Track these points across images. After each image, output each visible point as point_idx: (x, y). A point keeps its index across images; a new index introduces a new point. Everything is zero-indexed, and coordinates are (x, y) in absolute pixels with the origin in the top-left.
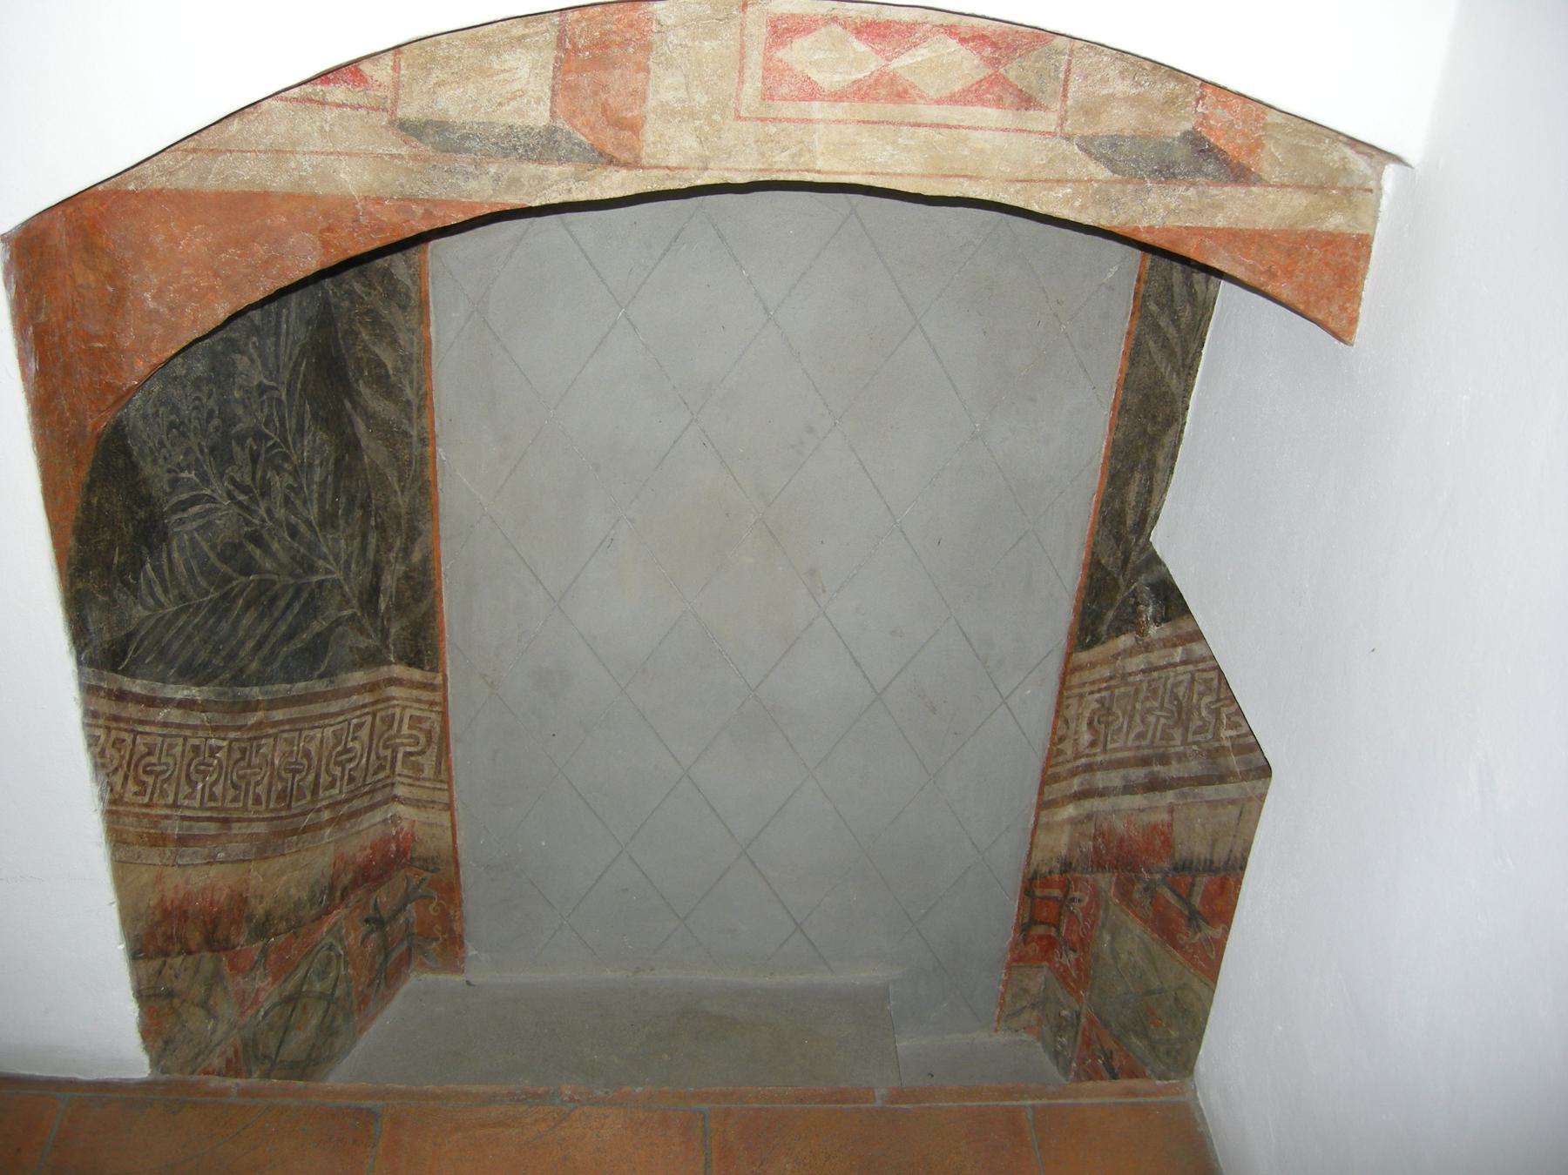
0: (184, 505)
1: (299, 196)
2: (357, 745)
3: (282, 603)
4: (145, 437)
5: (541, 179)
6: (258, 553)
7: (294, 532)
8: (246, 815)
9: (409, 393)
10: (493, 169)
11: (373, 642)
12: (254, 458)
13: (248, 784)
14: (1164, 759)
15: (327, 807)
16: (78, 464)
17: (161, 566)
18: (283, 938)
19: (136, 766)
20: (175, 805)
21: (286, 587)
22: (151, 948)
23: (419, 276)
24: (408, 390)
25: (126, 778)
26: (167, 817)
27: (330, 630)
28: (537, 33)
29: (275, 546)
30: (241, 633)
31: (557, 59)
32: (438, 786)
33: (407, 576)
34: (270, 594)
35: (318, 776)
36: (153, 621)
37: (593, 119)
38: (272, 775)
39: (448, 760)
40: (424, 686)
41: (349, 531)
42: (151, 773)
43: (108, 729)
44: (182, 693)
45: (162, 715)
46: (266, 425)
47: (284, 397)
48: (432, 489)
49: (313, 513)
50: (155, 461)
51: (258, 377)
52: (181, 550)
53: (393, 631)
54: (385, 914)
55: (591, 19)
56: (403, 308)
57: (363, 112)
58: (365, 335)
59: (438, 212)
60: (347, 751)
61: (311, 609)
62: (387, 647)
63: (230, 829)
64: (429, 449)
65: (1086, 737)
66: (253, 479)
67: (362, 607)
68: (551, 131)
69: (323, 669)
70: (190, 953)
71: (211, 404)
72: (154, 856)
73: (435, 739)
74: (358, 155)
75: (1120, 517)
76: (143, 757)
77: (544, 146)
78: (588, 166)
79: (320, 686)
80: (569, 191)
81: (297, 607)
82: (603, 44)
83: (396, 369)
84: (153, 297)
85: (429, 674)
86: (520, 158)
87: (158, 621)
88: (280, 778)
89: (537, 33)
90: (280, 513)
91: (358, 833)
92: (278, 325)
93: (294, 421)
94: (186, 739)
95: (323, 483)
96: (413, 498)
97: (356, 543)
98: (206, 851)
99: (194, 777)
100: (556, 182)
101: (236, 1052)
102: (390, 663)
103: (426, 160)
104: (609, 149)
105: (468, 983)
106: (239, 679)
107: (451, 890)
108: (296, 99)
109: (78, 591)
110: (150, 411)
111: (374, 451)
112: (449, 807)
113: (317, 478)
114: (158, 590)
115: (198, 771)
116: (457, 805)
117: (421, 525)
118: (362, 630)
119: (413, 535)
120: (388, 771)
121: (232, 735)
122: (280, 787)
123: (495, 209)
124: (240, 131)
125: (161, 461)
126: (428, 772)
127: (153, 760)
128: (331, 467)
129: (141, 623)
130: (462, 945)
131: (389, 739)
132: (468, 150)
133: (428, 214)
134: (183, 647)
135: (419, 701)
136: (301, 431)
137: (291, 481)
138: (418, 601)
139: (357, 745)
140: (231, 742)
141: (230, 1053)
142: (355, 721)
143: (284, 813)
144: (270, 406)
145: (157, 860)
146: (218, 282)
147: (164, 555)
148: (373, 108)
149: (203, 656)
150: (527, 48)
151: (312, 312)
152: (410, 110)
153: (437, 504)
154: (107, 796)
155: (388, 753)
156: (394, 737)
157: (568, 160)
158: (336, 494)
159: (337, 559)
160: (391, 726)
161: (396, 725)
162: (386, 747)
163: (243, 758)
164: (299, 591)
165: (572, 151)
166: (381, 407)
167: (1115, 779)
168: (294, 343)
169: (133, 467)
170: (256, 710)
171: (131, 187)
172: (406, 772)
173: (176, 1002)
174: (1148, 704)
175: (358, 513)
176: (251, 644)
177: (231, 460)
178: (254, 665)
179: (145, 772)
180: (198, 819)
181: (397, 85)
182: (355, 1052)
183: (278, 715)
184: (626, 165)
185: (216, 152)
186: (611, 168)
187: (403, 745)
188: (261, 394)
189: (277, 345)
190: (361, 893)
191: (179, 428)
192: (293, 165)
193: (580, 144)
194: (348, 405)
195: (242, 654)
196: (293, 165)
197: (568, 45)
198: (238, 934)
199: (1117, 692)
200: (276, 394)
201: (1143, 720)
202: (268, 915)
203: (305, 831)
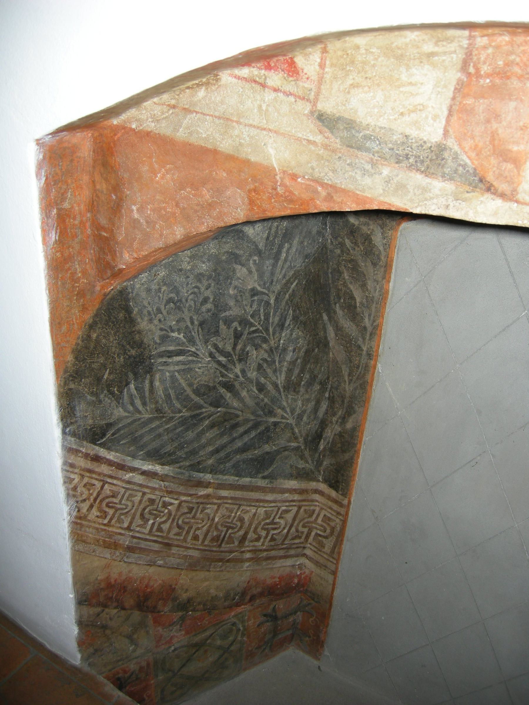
0: (170, 354)
1: (237, 158)
2: (282, 522)
3: (241, 430)
4: (145, 303)
5: (425, 190)
6: (228, 395)
7: (261, 388)
8: (184, 544)
9: (367, 322)
10: (386, 171)
11: (310, 466)
12: (237, 336)
13: (190, 528)
15: (250, 551)
16: (84, 309)
17: (143, 388)
18: (198, 614)
19: (101, 501)
20: (128, 528)
21: (247, 421)
22: (94, 601)
23: (388, 246)
24: (366, 320)
25: (91, 506)
26: (120, 534)
27: (278, 452)
28: (445, 53)
29: (244, 393)
30: (203, 441)
31: (459, 81)
32: (331, 559)
33: (340, 435)
34: (233, 422)
35: (246, 533)
36: (129, 420)
37: (481, 144)
38: (210, 526)
39: (340, 548)
40: (336, 502)
41: (307, 396)
42: (112, 507)
43: (82, 476)
44: (147, 467)
45: (128, 476)
46: (252, 316)
47: (272, 301)
48: (368, 388)
49: (281, 379)
50: (151, 321)
51: (252, 283)
52: (162, 381)
53: (325, 463)
54: (279, 614)
55: (498, 47)
56: (374, 264)
57: (292, 99)
58: (346, 275)
59: (337, 197)
60: (273, 523)
61: (266, 436)
62: (319, 471)
63: (170, 549)
64: (372, 362)
66: (234, 348)
67: (306, 442)
68: (441, 148)
69: (266, 473)
70: (123, 609)
71: (208, 293)
72: (107, 554)
73: (336, 533)
74: (283, 134)
76: (107, 497)
77: (431, 160)
78: (467, 188)
79: (261, 483)
80: (447, 207)
81: (253, 434)
82: (504, 74)
83: (361, 303)
84: (138, 210)
85: (340, 497)
86: (410, 167)
87: (135, 421)
88: (217, 529)
89: (445, 53)
90: (253, 374)
91: (272, 568)
92: (279, 253)
93: (277, 319)
94: (144, 494)
95: (293, 363)
96: (355, 389)
97: (311, 406)
98: (149, 558)
99: (147, 516)
100: (437, 196)
101: (148, 665)
102: (318, 481)
103: (334, 151)
104: (490, 177)
105: (319, 667)
106: (196, 467)
107: (324, 616)
108: (245, 79)
109: (70, 389)
110: (154, 287)
111: (336, 351)
112: (334, 573)
113: (288, 358)
114: (138, 402)
115: (150, 513)
116: (339, 574)
117: (356, 408)
118: (302, 457)
119: (350, 412)
120: (302, 540)
121: (184, 498)
122: (215, 533)
123: (382, 208)
124: (204, 98)
125: (156, 322)
126: (327, 549)
127: (115, 500)
128: (302, 354)
129: (120, 419)
130: (322, 646)
131: (308, 522)
132: (368, 150)
133: (329, 198)
134: (153, 440)
135: (331, 508)
136: (281, 326)
137: (266, 356)
138: (344, 452)
139: (282, 522)
140: (181, 502)
141: (144, 664)
142: (284, 508)
143: (214, 549)
144: (259, 305)
145: (108, 556)
146: (178, 211)
147: (147, 382)
148: (299, 97)
149: (169, 448)
150: (434, 66)
151: (311, 249)
152: (327, 106)
153: (369, 398)
154: (75, 514)
155: (306, 530)
156: (312, 522)
157: (451, 179)
158: (302, 371)
159: (293, 411)
160: (311, 516)
161: (315, 516)
162: (304, 526)
163: (190, 512)
164: (256, 426)
165: (456, 171)
166: (347, 325)
168: (290, 267)
169: (131, 321)
170: (207, 487)
171: (134, 126)
172: (314, 544)
173: (108, 632)
175: (317, 387)
176: (211, 449)
177: (217, 333)
178: (210, 462)
179: (107, 505)
180: (146, 540)
181: (321, 80)
182: (237, 680)
183: (224, 493)
184: (503, 196)
185: (187, 111)
186: (488, 196)
187: (316, 528)
188: (253, 296)
189: (274, 266)
190: (264, 600)
191: (177, 304)
192: (236, 132)
193: (464, 166)
194: (325, 317)
195: (202, 453)
196: (236, 132)
197: (472, 70)
198: (164, 605)
200: (265, 298)
202: (189, 600)
203: (228, 561)
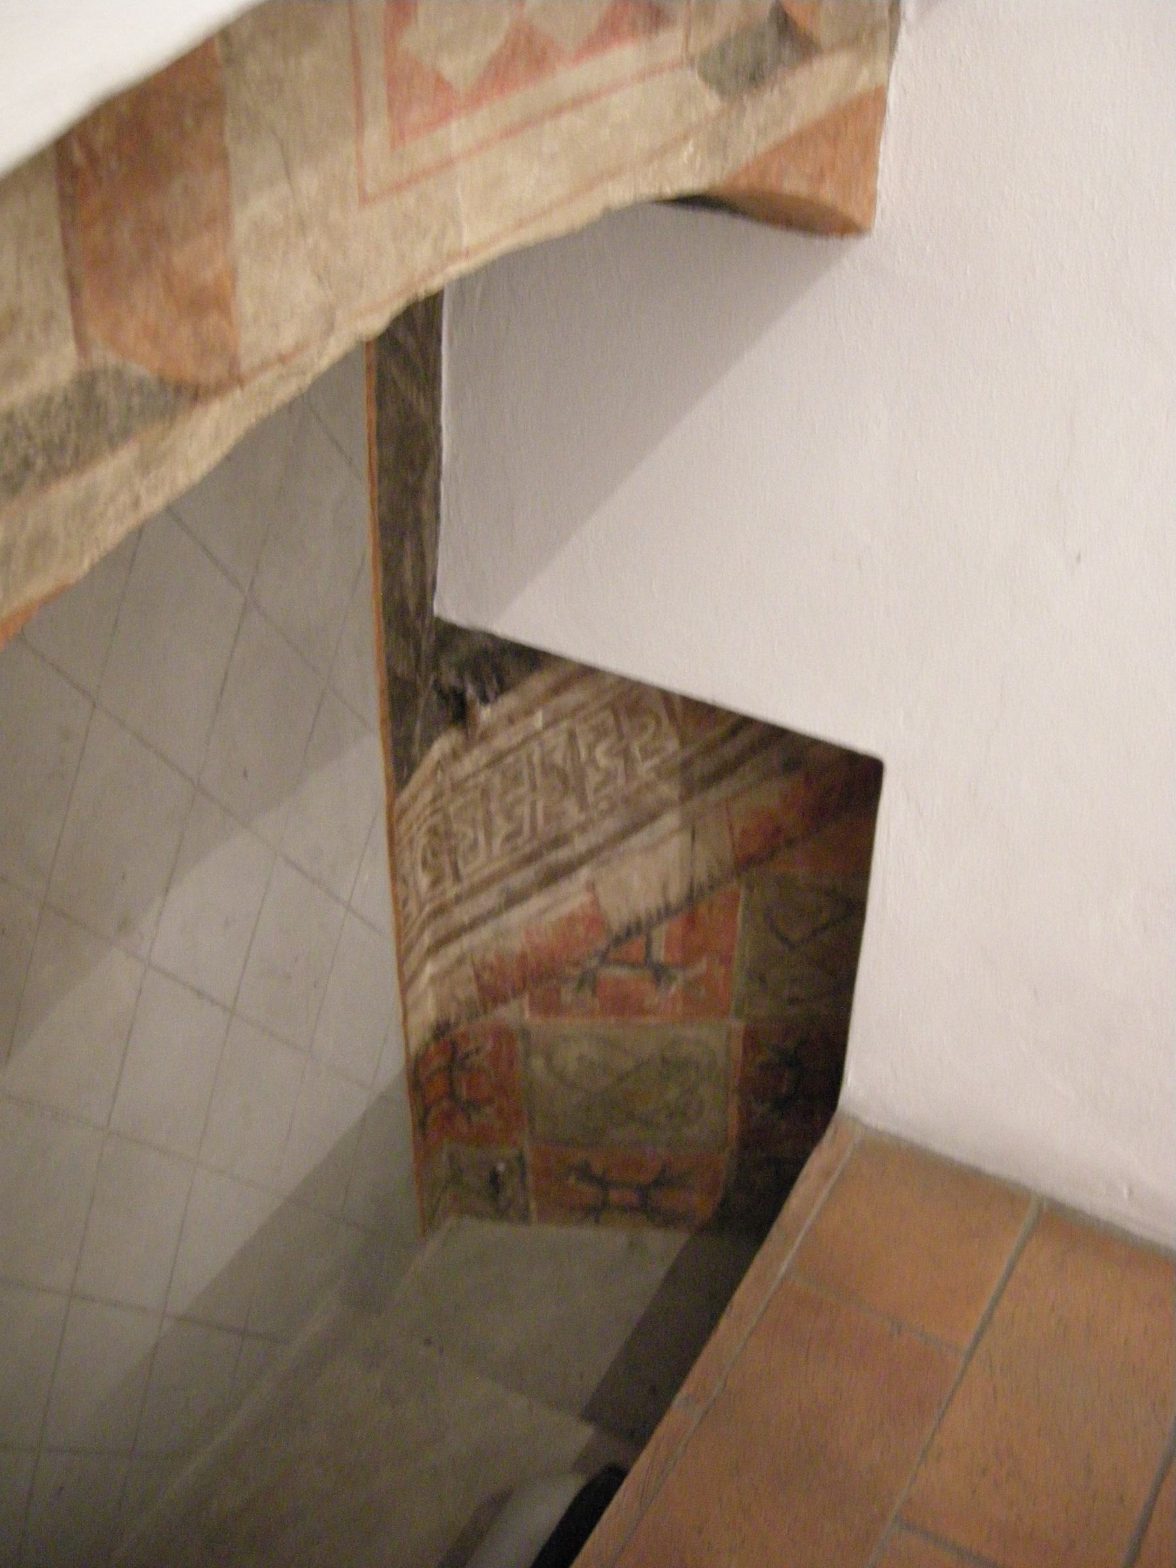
14: (559, 841)
65: (424, 880)
68: (87, 382)
75: (402, 608)
167: (488, 900)
174: (510, 798)
199: (452, 810)
201: (509, 817)
